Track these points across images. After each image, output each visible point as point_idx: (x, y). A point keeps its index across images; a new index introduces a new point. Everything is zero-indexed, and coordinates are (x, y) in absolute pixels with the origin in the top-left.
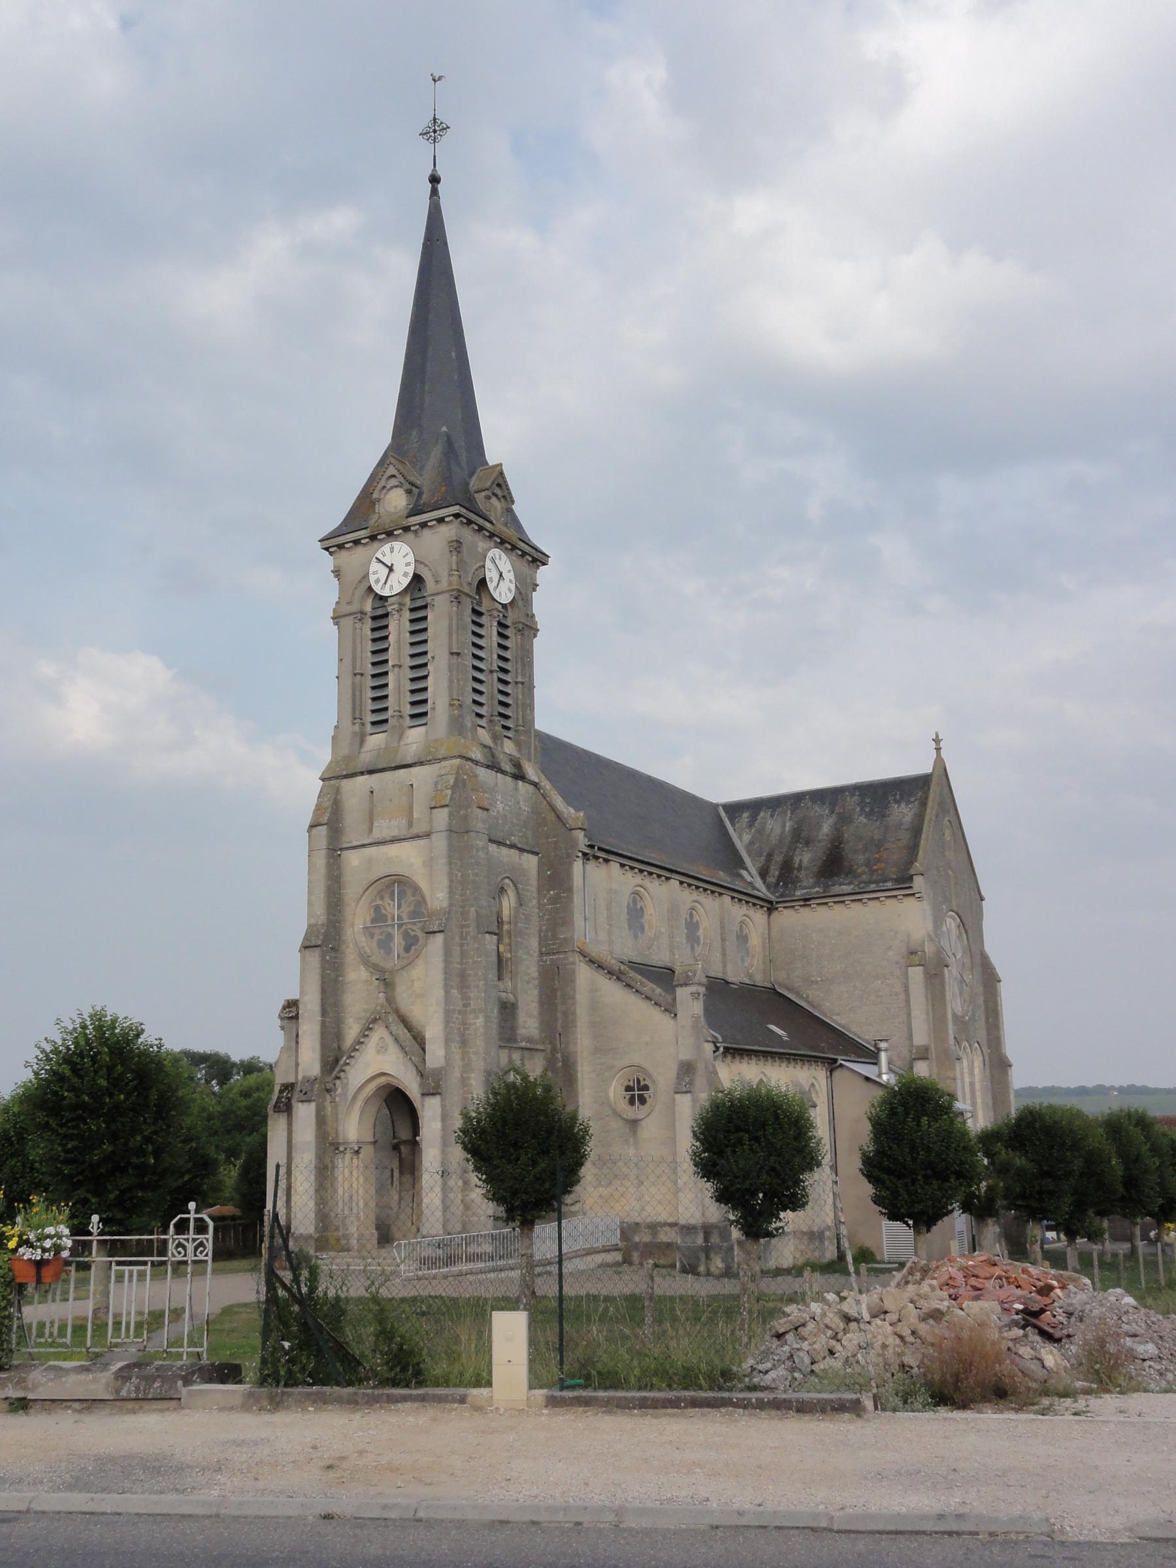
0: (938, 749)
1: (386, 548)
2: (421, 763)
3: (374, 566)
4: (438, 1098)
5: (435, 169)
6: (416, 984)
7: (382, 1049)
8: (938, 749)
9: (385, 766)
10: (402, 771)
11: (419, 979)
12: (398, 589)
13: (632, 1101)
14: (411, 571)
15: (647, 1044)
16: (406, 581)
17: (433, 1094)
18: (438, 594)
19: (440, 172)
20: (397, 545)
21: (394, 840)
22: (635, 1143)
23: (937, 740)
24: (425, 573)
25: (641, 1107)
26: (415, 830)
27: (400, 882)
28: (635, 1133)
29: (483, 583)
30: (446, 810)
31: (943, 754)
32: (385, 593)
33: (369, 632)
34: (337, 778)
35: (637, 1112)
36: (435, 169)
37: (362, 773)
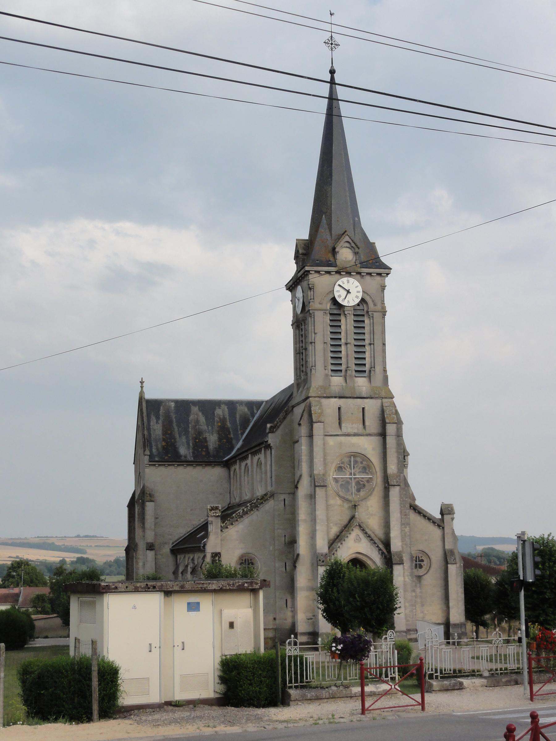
0: (142, 387)
1: (345, 279)
2: (371, 398)
3: (337, 288)
4: (401, 566)
5: (332, 66)
6: (370, 509)
7: (358, 540)
8: (142, 387)
9: (350, 396)
10: (359, 400)
11: (371, 506)
12: (352, 304)
13: (416, 567)
14: (360, 295)
15: (426, 540)
16: (357, 301)
17: (400, 564)
18: (376, 312)
19: (335, 68)
20: (351, 280)
21: (355, 435)
22: (420, 587)
23: (142, 382)
24: (367, 299)
25: (420, 570)
26: (368, 431)
27: (354, 456)
28: (420, 582)
29: (334, 301)
30: (395, 425)
31: (144, 389)
32: (345, 303)
33: (329, 321)
34: (319, 397)
35: (421, 572)
36: (332, 66)
37: (335, 397)
